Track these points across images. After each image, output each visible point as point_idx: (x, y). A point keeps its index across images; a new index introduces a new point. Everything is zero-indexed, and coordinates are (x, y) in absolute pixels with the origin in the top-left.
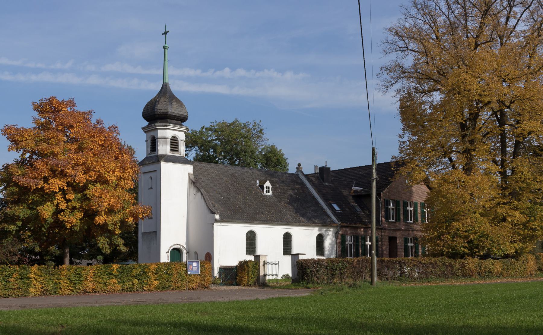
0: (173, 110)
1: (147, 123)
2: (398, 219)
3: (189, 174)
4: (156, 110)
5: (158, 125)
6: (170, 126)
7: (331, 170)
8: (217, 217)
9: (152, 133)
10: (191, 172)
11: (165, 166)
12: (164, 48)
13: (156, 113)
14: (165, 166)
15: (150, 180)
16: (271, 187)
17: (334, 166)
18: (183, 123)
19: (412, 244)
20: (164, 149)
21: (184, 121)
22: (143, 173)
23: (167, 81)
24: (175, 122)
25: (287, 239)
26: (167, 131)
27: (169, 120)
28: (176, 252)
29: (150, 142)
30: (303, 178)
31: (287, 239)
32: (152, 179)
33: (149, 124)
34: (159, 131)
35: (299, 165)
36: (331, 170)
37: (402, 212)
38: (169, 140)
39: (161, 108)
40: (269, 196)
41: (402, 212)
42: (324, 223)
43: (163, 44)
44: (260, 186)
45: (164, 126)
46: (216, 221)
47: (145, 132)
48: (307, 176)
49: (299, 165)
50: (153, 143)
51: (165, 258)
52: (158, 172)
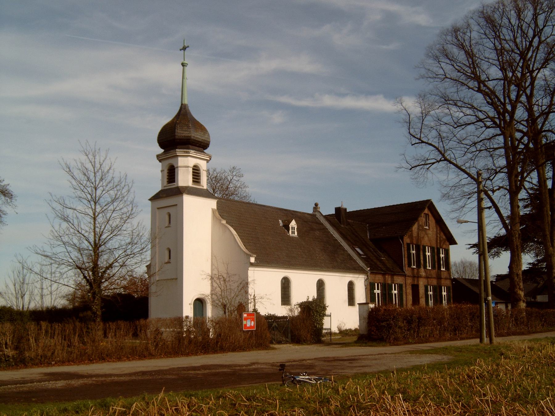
0: (196, 135)
1: (162, 151)
2: (419, 266)
3: (213, 209)
4: (176, 134)
5: (179, 152)
6: (192, 152)
7: (348, 211)
8: (252, 260)
9: (171, 161)
10: (215, 206)
11: (188, 200)
12: (183, 65)
13: (177, 137)
14: (188, 200)
15: (167, 217)
16: (296, 227)
17: (350, 209)
18: (205, 151)
19: (379, 291)
20: (184, 179)
21: (206, 148)
22: (158, 208)
23: (186, 102)
24: (197, 148)
25: (286, 284)
26: (189, 158)
27: (190, 146)
28: (199, 303)
29: (166, 171)
30: (323, 221)
31: (286, 284)
32: (170, 215)
33: (164, 152)
34: (180, 159)
35: (316, 205)
36: (348, 211)
37: (422, 258)
38: (191, 170)
39: (181, 133)
40: (295, 237)
41: (422, 258)
42: (355, 269)
43: (182, 61)
44: (284, 226)
45: (187, 152)
46: (252, 265)
47: (160, 161)
48: (327, 217)
49: (316, 205)
50: (171, 174)
51: (188, 311)
52: (179, 207)
